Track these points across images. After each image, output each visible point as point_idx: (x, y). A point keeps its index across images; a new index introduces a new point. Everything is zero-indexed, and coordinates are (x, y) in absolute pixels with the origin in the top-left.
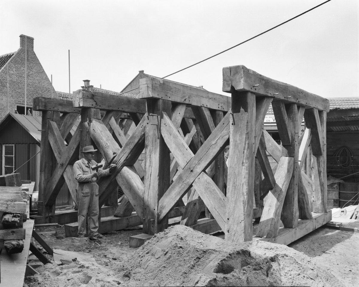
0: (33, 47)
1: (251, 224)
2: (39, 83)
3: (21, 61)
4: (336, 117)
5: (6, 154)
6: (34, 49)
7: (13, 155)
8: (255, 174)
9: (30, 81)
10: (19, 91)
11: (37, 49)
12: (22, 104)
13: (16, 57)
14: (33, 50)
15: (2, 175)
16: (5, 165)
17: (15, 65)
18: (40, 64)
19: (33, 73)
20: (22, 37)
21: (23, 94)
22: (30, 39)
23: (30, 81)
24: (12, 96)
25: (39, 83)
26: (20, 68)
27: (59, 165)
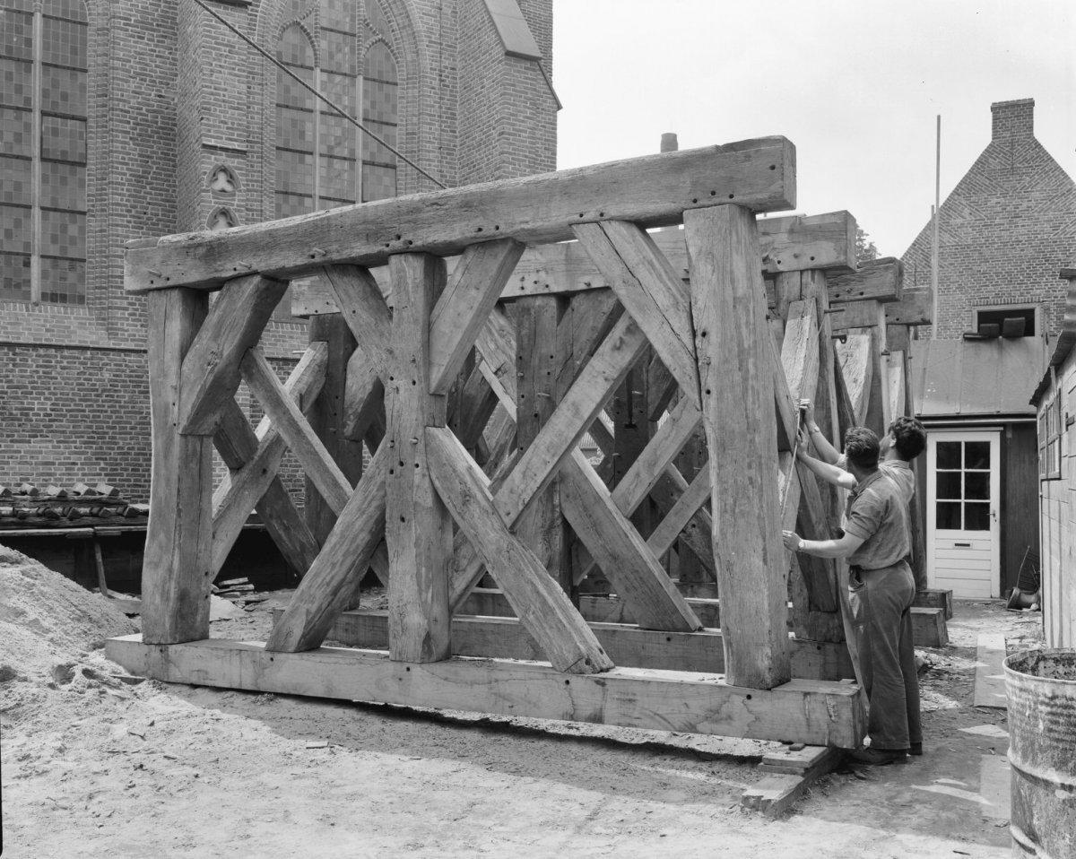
0: (1031, 128)
1: (1036, 680)
2: (1055, 228)
3: (987, 182)
4: (709, 267)
5: (986, 477)
6: (1034, 131)
7: (966, 473)
8: (830, 408)
9: (1022, 230)
10: (984, 268)
11: (1045, 131)
12: (994, 304)
13: (972, 175)
14: (1031, 135)
15: (939, 526)
16: (939, 496)
17: (967, 199)
18: (1058, 168)
19: (1032, 204)
20: (1029, 104)
21: (996, 273)
22: (1019, 106)
23: (1022, 230)
24: (960, 287)
25: (1055, 228)
26: (986, 201)
27: (313, 260)
